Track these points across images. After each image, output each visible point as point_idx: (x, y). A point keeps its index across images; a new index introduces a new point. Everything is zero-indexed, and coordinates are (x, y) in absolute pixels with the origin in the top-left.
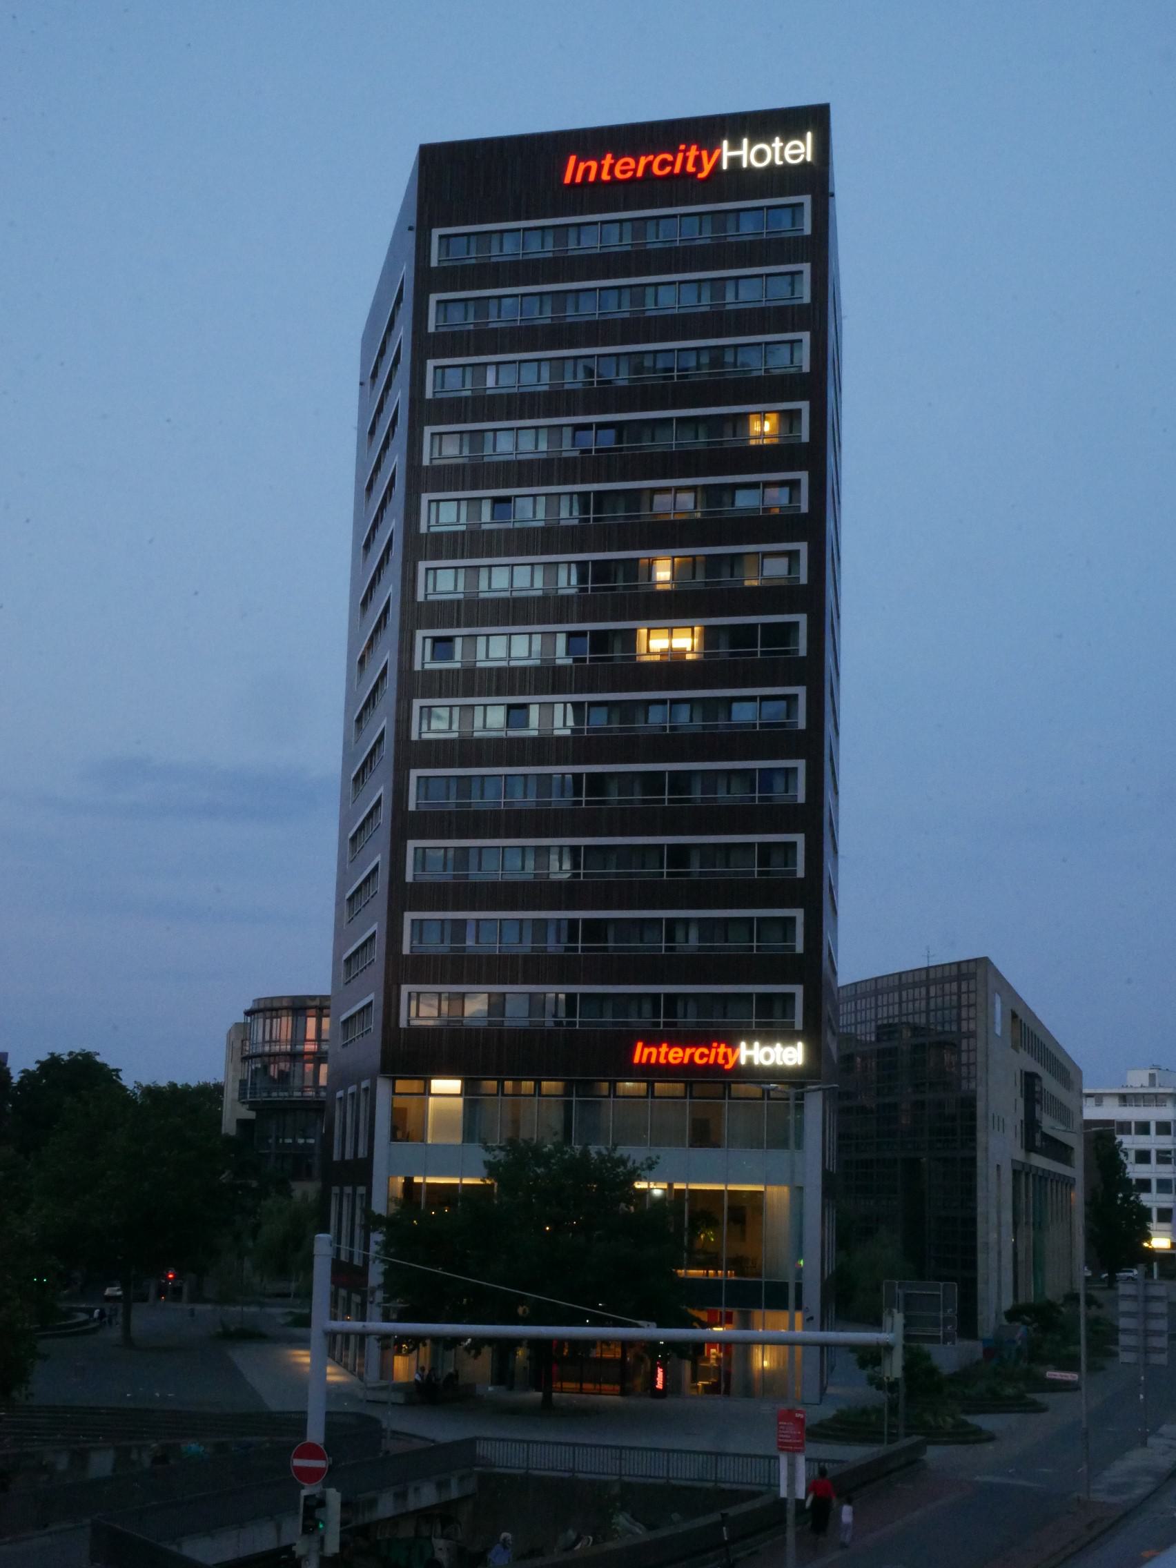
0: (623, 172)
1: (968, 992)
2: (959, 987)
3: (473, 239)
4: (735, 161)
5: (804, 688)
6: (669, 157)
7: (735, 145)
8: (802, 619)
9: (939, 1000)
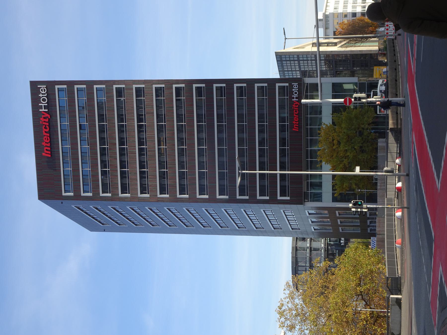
0: (48, 139)
1: (293, 58)
2: (284, 61)
6: (44, 126)
9: (286, 65)
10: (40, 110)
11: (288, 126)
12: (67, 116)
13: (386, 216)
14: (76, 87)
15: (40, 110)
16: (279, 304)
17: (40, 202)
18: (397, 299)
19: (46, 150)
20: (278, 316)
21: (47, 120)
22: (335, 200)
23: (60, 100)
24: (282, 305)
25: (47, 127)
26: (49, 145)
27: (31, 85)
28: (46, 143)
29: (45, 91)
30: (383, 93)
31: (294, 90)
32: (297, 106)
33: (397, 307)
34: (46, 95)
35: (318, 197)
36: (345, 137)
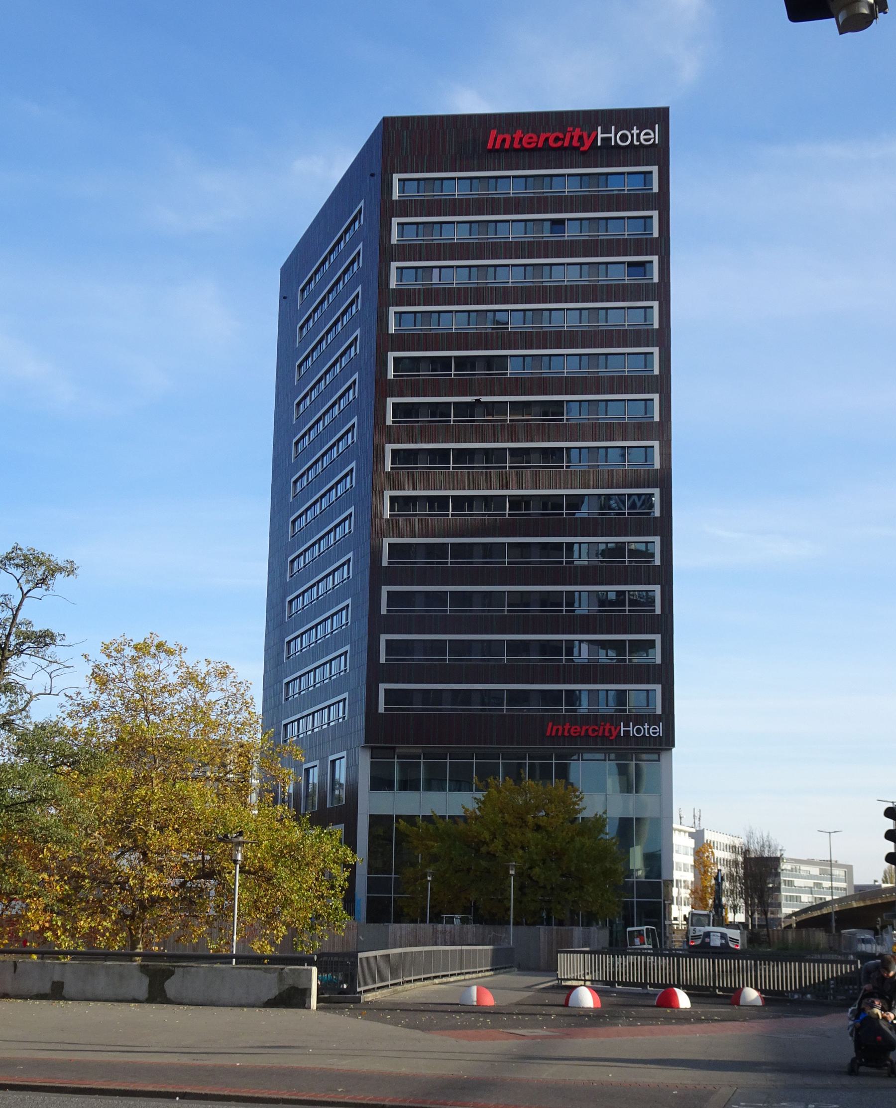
0: (529, 143)
3: (421, 226)
4: (606, 140)
5: (657, 167)
6: (561, 136)
7: (606, 130)
8: (655, 259)
10: (599, 128)
11: (558, 710)
12: (586, 190)
13: (459, 948)
14: (655, 214)
15: (599, 128)
16: (171, 645)
17: (380, 118)
18: (307, 992)
19: (504, 140)
20: (138, 639)
21: (575, 143)
22: (375, 820)
23: (622, 177)
24: (170, 652)
25: (559, 144)
26: (516, 145)
27: (659, 109)
28: (521, 139)
29: (646, 140)
30: (703, 941)
31: (646, 726)
32: (607, 734)
33: (274, 992)
34: (636, 143)
35: (380, 783)
36: (558, 845)
